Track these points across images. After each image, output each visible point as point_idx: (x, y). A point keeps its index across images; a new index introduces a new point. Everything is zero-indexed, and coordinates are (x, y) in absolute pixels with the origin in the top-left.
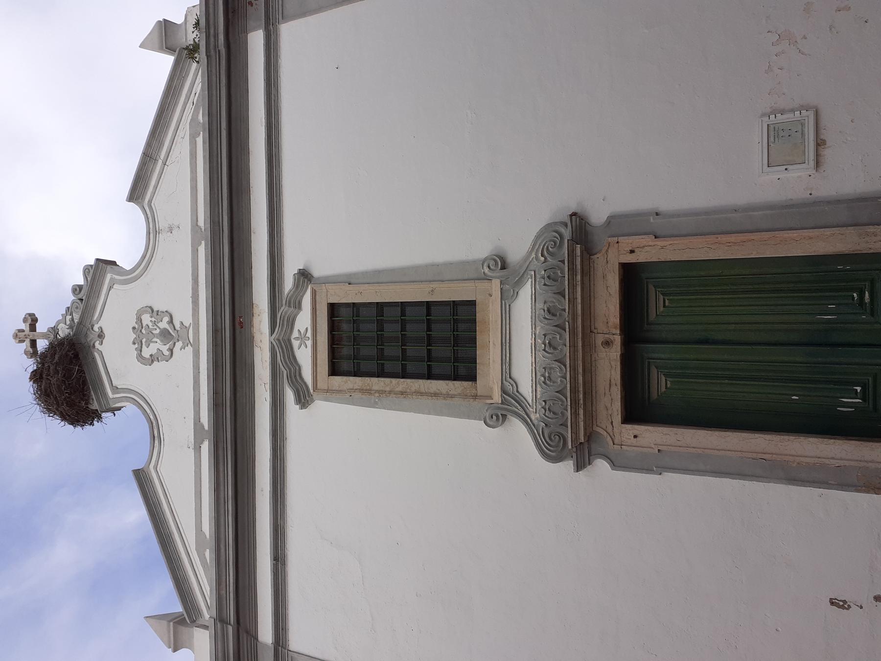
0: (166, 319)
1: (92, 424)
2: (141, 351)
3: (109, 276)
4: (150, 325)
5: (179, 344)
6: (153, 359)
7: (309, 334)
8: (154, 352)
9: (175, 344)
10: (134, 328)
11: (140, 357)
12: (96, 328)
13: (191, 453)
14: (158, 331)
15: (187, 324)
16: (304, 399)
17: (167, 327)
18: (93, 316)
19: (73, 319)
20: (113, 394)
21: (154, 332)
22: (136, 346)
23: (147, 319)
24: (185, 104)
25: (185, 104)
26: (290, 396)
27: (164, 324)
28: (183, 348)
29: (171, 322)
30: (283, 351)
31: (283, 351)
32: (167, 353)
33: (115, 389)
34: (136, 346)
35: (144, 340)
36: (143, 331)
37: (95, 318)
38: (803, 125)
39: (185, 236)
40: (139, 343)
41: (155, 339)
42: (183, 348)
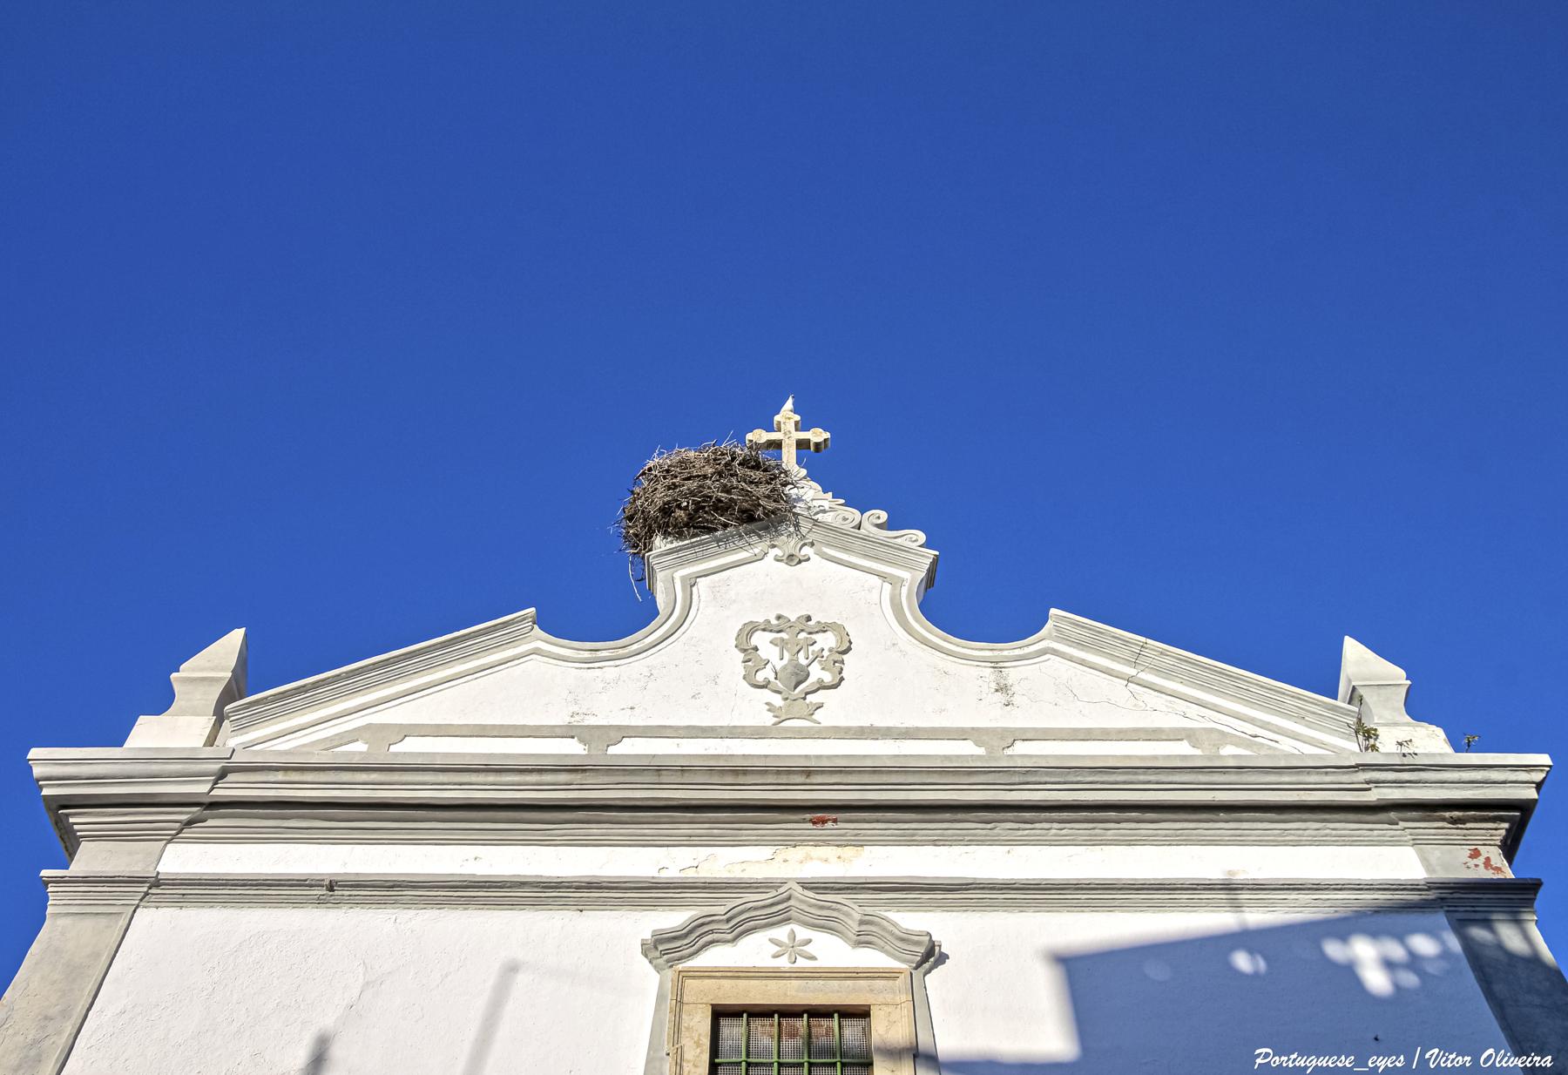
0: (828, 678)
3: (905, 574)
4: (816, 648)
5: (777, 700)
7: (802, 963)
8: (762, 653)
12: (807, 550)
13: (560, 718)
14: (803, 661)
15: (818, 715)
16: (663, 948)
18: (829, 545)
19: (824, 512)
20: (683, 579)
21: (801, 654)
22: (774, 622)
23: (827, 641)
24: (1252, 721)
25: (1252, 721)
26: (674, 919)
27: (816, 673)
28: (771, 707)
29: (822, 687)
30: (764, 907)
31: (764, 907)
32: (760, 677)
33: (690, 582)
34: (774, 622)
35: (783, 635)
36: (803, 635)
39: (992, 716)
40: (779, 625)
42: (771, 707)
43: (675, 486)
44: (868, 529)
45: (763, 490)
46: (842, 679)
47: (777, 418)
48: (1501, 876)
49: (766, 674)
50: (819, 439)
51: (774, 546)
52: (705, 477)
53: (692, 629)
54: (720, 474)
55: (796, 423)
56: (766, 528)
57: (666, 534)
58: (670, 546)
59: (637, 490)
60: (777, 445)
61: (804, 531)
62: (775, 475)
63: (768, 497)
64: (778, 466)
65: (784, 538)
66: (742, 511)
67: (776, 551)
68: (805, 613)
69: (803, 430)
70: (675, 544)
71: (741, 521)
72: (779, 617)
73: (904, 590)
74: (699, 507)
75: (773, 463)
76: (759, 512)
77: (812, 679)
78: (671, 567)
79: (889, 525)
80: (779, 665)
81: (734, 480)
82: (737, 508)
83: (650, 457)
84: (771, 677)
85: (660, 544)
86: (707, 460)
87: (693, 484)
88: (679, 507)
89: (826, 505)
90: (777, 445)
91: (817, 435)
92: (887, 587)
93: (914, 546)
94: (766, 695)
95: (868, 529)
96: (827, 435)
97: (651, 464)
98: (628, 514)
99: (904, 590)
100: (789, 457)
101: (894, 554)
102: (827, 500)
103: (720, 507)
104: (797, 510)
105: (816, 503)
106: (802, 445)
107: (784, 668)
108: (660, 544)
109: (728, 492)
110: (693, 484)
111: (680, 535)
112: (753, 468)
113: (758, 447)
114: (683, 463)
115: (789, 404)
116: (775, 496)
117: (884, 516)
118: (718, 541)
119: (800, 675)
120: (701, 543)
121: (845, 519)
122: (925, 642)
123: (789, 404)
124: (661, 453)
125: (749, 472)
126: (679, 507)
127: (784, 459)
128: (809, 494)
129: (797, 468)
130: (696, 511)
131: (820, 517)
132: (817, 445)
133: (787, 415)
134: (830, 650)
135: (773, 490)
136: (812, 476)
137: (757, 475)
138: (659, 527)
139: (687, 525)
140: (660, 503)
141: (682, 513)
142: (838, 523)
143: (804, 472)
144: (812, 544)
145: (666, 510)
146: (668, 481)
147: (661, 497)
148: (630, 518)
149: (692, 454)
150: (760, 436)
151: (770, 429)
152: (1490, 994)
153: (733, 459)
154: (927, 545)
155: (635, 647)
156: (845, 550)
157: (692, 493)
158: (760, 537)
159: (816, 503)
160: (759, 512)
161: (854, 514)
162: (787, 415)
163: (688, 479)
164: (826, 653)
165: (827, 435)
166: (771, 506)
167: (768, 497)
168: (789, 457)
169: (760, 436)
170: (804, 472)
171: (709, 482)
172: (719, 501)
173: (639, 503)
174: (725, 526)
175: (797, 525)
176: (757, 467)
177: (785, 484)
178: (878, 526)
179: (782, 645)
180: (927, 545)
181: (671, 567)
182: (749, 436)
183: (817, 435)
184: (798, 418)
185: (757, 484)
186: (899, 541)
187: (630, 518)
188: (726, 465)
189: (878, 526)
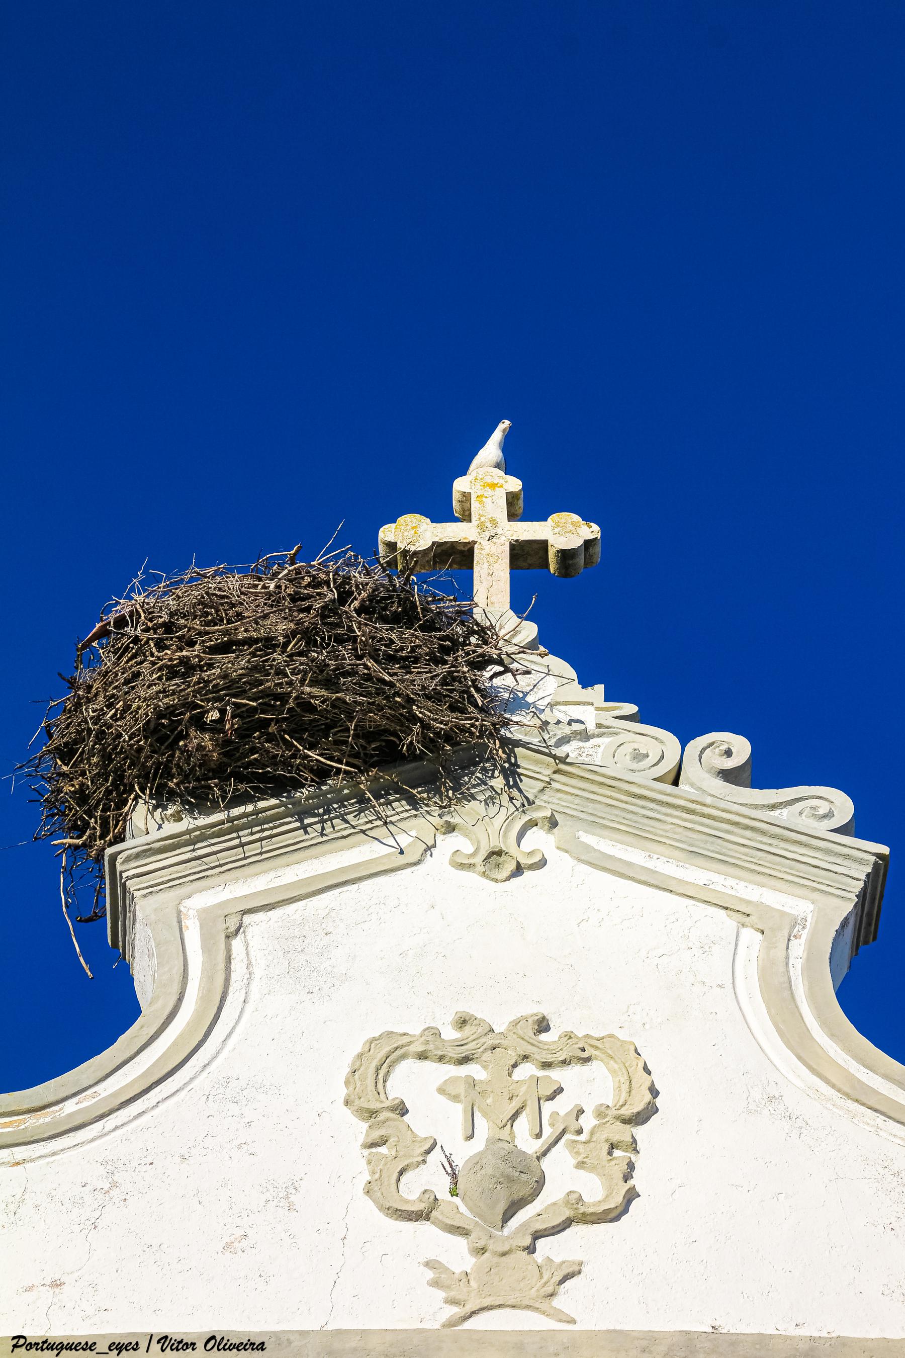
0: (594, 1191)
1: (586, 682)
2: (423, 1056)
3: (799, 906)
4: (562, 1106)
5: (457, 1254)
6: (383, 1118)
8: (419, 1123)
9: (461, 1231)
10: (543, 1026)
11: (386, 1054)
12: (538, 840)
14: (529, 1145)
15: (569, 1299)
17: (552, 1193)
18: (595, 825)
19: (585, 736)
20: (206, 917)
21: (523, 1125)
22: (450, 1034)
23: (590, 1088)
27: (565, 1178)
28: (440, 1275)
29: (579, 1216)
32: (412, 1190)
33: (230, 927)
34: (450, 1034)
35: (474, 1070)
36: (526, 1070)
37: (586, 838)
38: (397, 1210)
40: (463, 1046)
41: (483, 1126)
42: (440, 1275)
43: (188, 668)
44: (701, 780)
45: (424, 678)
46: (631, 1195)
47: (460, 485)
48: (401, 769)
49: (429, 1179)
50: (574, 542)
51: (450, 828)
52: (269, 643)
53: (239, 1049)
54: (309, 636)
55: (511, 498)
56: (431, 782)
57: (162, 797)
58: (172, 828)
59: (85, 676)
60: (460, 557)
61: (529, 787)
62: (458, 643)
63: (435, 697)
64: (465, 615)
65: (475, 807)
66: (367, 735)
67: (448, 844)
68: (532, 1009)
69: (525, 518)
70: (187, 823)
71: (363, 761)
72: (463, 1022)
73: (798, 948)
74: (250, 723)
75: (449, 606)
76: (412, 738)
77: (551, 1194)
78: (191, 900)
79: (760, 773)
80: (464, 1153)
81: (345, 651)
82: (376, 730)
83: (121, 590)
84: (441, 1186)
85: (145, 822)
86: (274, 599)
87: (236, 664)
88: (199, 722)
89: (589, 717)
90: (460, 557)
91: (565, 531)
92: (749, 936)
93: (822, 828)
94: (428, 1237)
95: (701, 780)
96: (592, 531)
97: (124, 607)
98: (57, 741)
99: (798, 948)
100: (491, 589)
101: (770, 851)
102: (590, 706)
103: (309, 724)
104: (514, 733)
105: (560, 714)
106: (526, 556)
107: (476, 1162)
108: (145, 822)
109: (330, 684)
110: (236, 664)
111: (200, 801)
112: (395, 620)
113: (413, 559)
114: (212, 608)
115: (491, 450)
116: (457, 695)
117: (741, 748)
118: (302, 813)
119: (518, 1185)
120: (256, 821)
121: (639, 756)
122: (858, 1095)
123: (491, 450)
124: (150, 580)
125: (384, 631)
126: (199, 722)
127: (479, 597)
128: (549, 691)
129: (512, 619)
130: (244, 733)
131: (570, 750)
132: (566, 556)
133: (486, 480)
134: (600, 1113)
135: (450, 679)
136: (551, 641)
137: (407, 638)
138: (145, 778)
139: (219, 772)
140: (145, 712)
141: (207, 740)
142: (620, 766)
143: (530, 630)
144: (553, 823)
145: (164, 731)
146: (172, 655)
147: (149, 695)
148: (66, 753)
149: (234, 583)
150: (413, 532)
151: (441, 511)
152: (158, 1060)
153: (344, 597)
154: (858, 828)
155: (70, 1107)
156: (639, 837)
157: (234, 687)
158: (414, 803)
159: (560, 714)
160: (412, 738)
161: (661, 743)
162: (486, 480)
163: (224, 648)
164: (588, 1122)
165: (592, 531)
166: (443, 720)
167: (435, 697)
168: (491, 589)
169: (413, 532)
170: (530, 630)
171: (278, 657)
172: (306, 706)
173: (89, 712)
174: (322, 774)
175: (512, 773)
176: (407, 616)
177: (481, 663)
178: (728, 775)
179: (472, 1098)
180: (858, 828)
181: (191, 900)
182: (387, 533)
183: (565, 531)
184: (515, 484)
185: (408, 662)
186: (783, 815)
187: (66, 753)
188: (325, 612)
189: (728, 775)
